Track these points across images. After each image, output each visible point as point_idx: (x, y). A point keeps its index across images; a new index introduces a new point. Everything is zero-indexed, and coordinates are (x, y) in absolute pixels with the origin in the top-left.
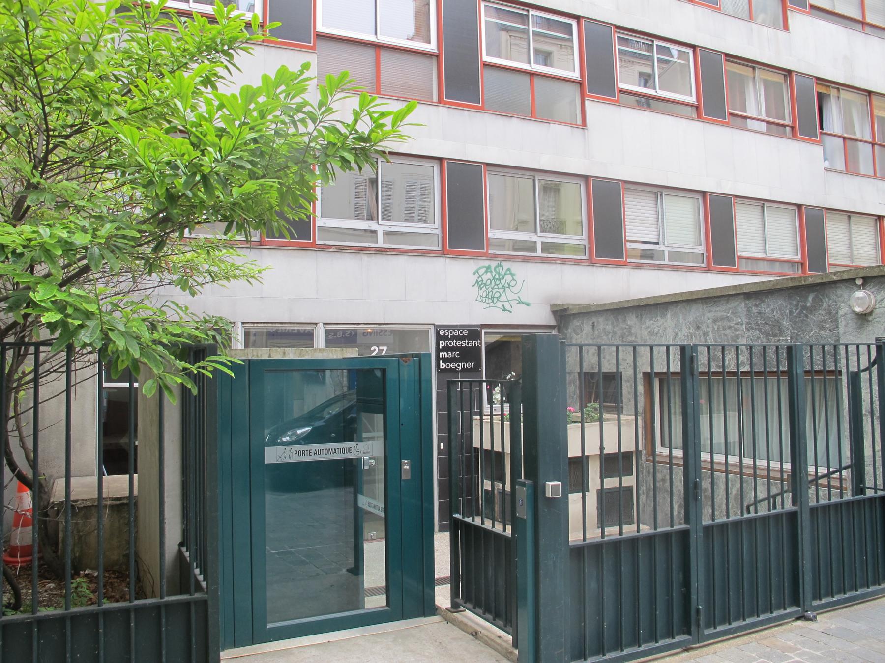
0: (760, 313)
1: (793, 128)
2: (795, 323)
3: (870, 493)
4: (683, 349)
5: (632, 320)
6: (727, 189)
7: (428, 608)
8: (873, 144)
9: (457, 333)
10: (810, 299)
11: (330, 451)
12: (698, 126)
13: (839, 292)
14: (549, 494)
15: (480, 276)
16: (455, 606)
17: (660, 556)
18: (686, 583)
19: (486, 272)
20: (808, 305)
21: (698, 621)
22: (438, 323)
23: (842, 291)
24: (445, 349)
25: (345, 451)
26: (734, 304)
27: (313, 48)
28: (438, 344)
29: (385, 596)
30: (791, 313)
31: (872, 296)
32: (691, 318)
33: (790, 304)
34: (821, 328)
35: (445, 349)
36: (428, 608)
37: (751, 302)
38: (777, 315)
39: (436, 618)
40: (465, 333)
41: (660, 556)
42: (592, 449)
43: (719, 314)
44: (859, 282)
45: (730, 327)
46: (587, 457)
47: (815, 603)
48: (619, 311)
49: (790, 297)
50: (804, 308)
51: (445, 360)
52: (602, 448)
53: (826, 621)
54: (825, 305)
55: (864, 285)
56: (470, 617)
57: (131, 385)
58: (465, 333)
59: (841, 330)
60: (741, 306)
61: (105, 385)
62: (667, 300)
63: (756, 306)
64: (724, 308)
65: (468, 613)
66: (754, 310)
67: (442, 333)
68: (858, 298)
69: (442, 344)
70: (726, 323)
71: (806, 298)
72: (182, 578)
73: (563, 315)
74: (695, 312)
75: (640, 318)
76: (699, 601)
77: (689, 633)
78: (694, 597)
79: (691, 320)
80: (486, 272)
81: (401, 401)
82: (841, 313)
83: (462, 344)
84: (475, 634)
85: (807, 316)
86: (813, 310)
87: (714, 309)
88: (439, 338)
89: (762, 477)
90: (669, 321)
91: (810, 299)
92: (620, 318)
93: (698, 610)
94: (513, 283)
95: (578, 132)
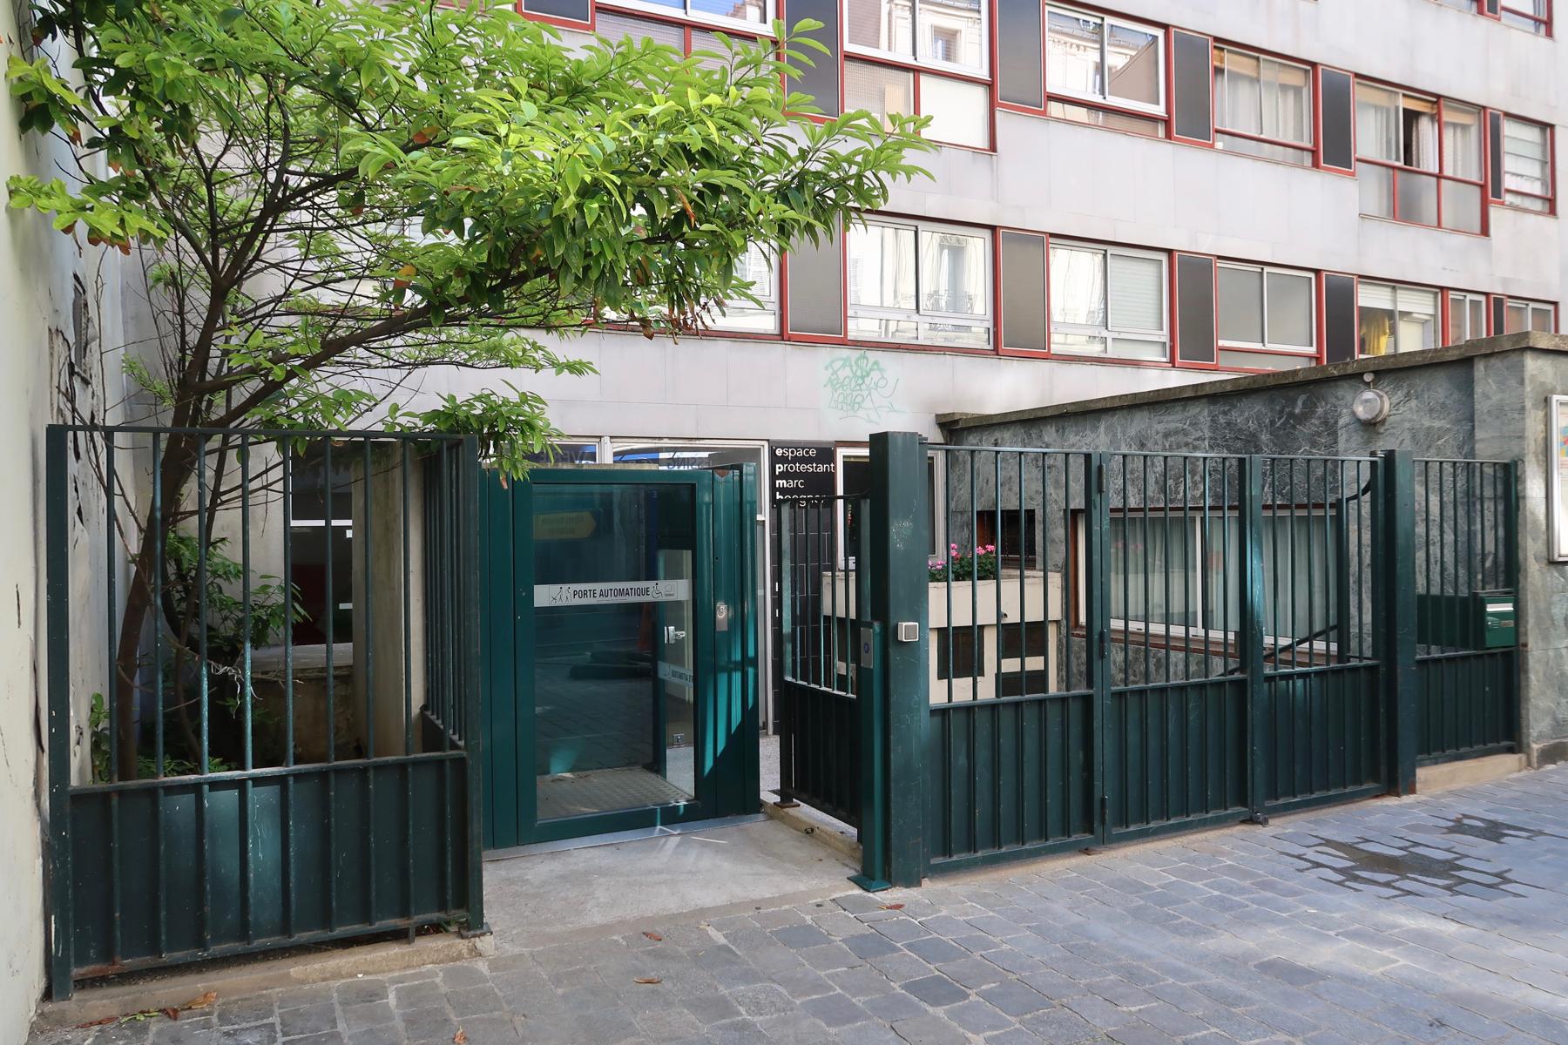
0: (1228, 424)
1: (1314, 153)
2: (1277, 437)
3: (1354, 663)
4: (1088, 457)
5: (1050, 433)
6: (1206, 244)
7: (749, 804)
8: (1439, 177)
9: (801, 453)
10: (1300, 403)
11: (621, 592)
12: (1167, 149)
13: (1340, 393)
14: (902, 637)
15: (835, 372)
16: (786, 794)
17: (1054, 729)
18: (1088, 766)
19: (843, 366)
20: (1297, 411)
21: (1103, 814)
22: (772, 438)
23: (1344, 391)
24: (783, 476)
25: (639, 592)
26: (1193, 410)
27: (592, 27)
28: (773, 469)
29: (691, 750)
30: (1272, 423)
31: (1386, 398)
32: (1132, 432)
33: (1272, 410)
34: (1314, 444)
35: (783, 476)
36: (749, 804)
37: (1218, 408)
38: (1252, 426)
39: (761, 817)
40: (813, 453)
41: (1054, 729)
42: (987, 616)
43: (1172, 426)
44: (1368, 378)
45: (1187, 444)
46: (982, 627)
47: (1268, 804)
48: (1030, 421)
49: (1272, 401)
50: (1291, 415)
51: (783, 491)
52: (1000, 615)
53: (1280, 826)
54: (1320, 410)
55: (1374, 384)
56: (806, 812)
57: (328, 523)
58: (813, 453)
59: (1341, 445)
60: (1202, 413)
61: (294, 523)
62: (1099, 406)
63: (1225, 413)
64: (1179, 417)
65: (805, 808)
66: (1222, 419)
67: (779, 452)
68: (1367, 401)
69: (779, 468)
70: (1181, 439)
71: (1294, 402)
72: (431, 736)
73: (953, 428)
74: (1140, 423)
75: (1061, 431)
76: (1105, 788)
77: (1092, 832)
78: (1098, 783)
79: (1133, 433)
80: (843, 366)
81: (712, 528)
82: (1341, 422)
83: (805, 472)
84: (810, 831)
85: (1294, 427)
86: (1303, 418)
87: (1166, 418)
88: (775, 460)
89: (1217, 654)
90: (1102, 436)
91: (1300, 403)
92: (1034, 432)
93: (1103, 801)
94: (882, 383)
95: (983, 160)
